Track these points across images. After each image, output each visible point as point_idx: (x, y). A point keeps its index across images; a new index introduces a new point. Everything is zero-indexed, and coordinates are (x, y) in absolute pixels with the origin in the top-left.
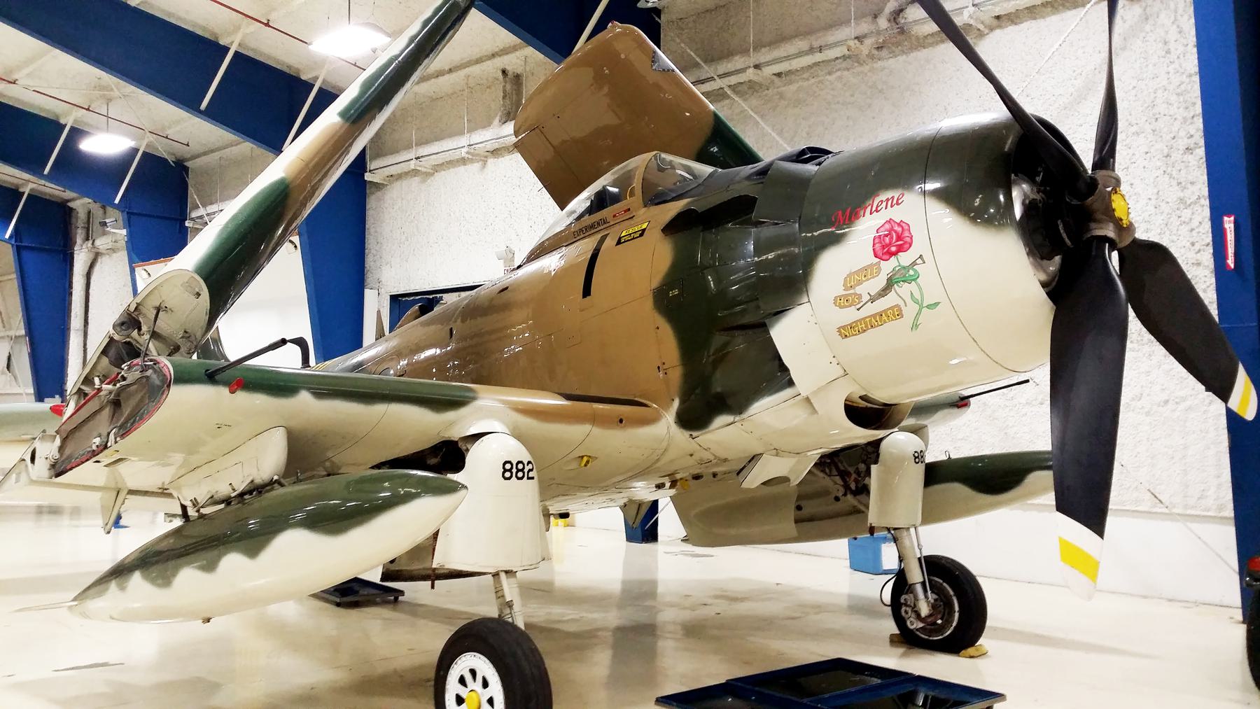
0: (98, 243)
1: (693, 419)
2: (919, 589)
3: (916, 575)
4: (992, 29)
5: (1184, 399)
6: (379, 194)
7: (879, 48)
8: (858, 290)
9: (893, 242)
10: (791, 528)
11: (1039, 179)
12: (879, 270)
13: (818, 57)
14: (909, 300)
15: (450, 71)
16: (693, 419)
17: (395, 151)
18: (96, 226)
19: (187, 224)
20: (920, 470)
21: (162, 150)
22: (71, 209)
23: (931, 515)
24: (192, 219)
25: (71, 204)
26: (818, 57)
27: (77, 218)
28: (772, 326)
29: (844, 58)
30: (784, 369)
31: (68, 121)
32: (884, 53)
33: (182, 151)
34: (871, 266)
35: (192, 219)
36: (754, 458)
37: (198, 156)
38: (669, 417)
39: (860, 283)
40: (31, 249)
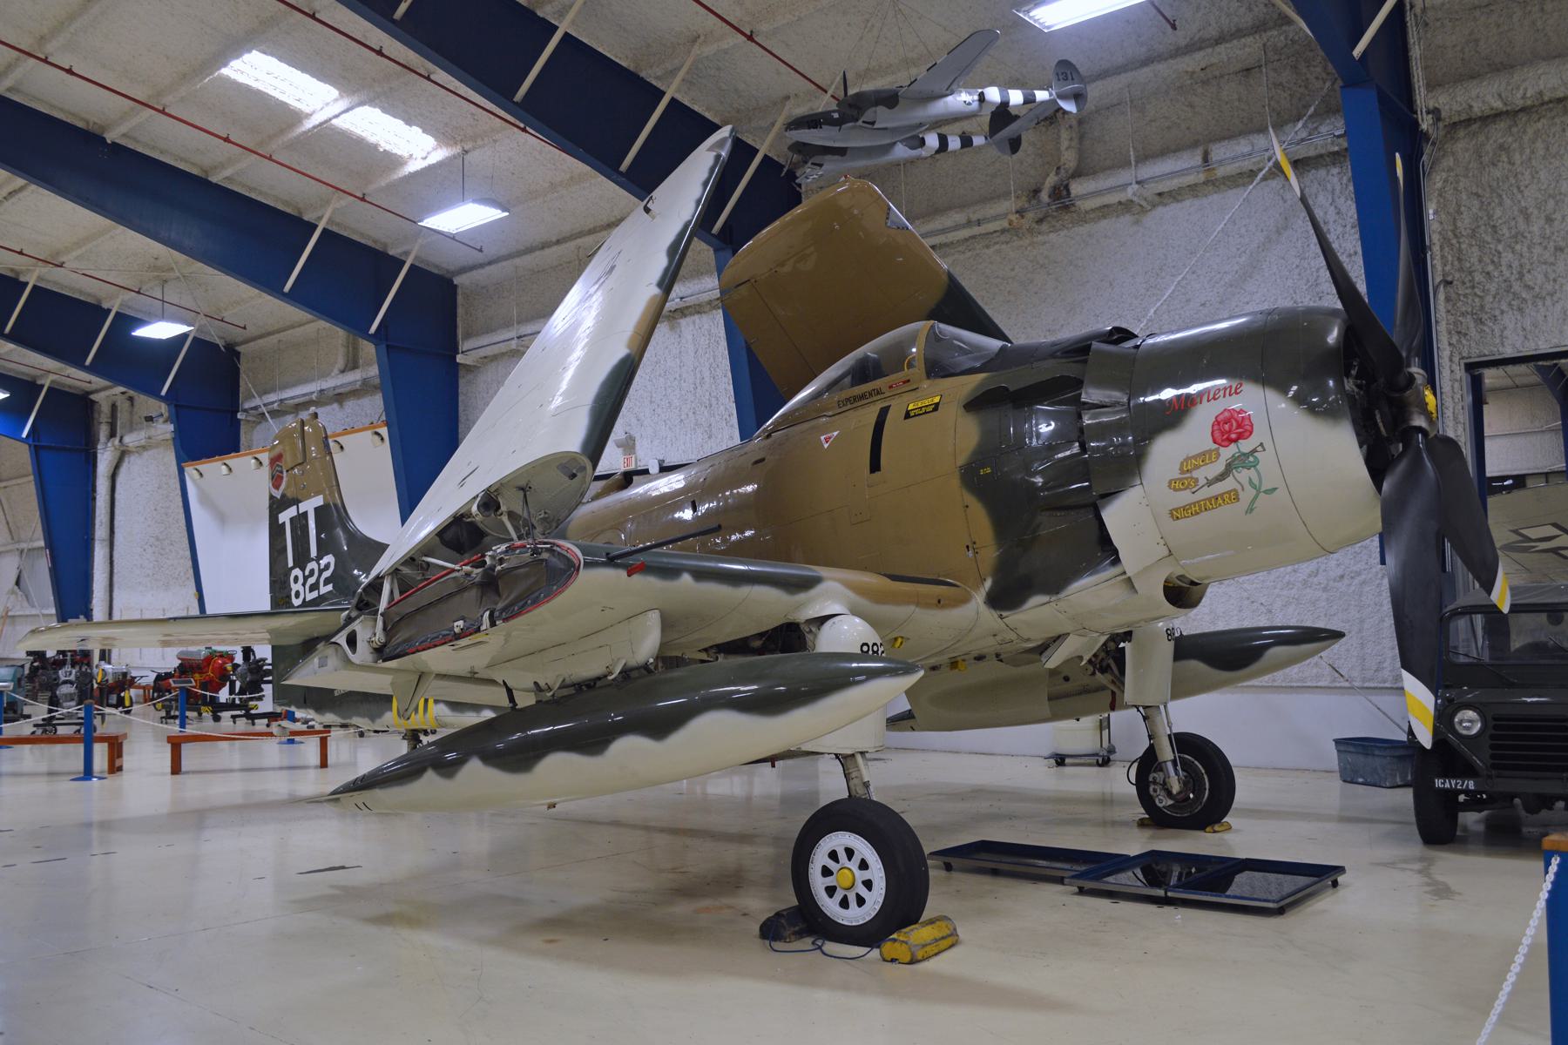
0: (127, 439)
1: (1005, 597)
2: (1170, 765)
3: (1166, 753)
4: (1154, 206)
5: (1359, 574)
6: (470, 377)
7: (1040, 221)
8: (1195, 474)
9: (1231, 429)
10: (1046, 709)
11: (1354, 372)
12: (1218, 455)
13: (976, 230)
14: (1247, 486)
15: (558, 242)
16: (1005, 597)
17: (489, 330)
18: (122, 417)
19: (239, 416)
20: (1169, 647)
21: (215, 335)
22: (93, 402)
23: (1181, 689)
24: (245, 411)
25: (93, 397)
26: (976, 230)
27: (100, 413)
28: (1104, 507)
29: (1003, 231)
30: (1116, 552)
31: (115, 304)
32: (1044, 227)
33: (236, 334)
34: (1210, 451)
35: (245, 411)
36: (1059, 639)
37: (254, 339)
38: (979, 598)
39: (1197, 467)
40: (50, 448)
